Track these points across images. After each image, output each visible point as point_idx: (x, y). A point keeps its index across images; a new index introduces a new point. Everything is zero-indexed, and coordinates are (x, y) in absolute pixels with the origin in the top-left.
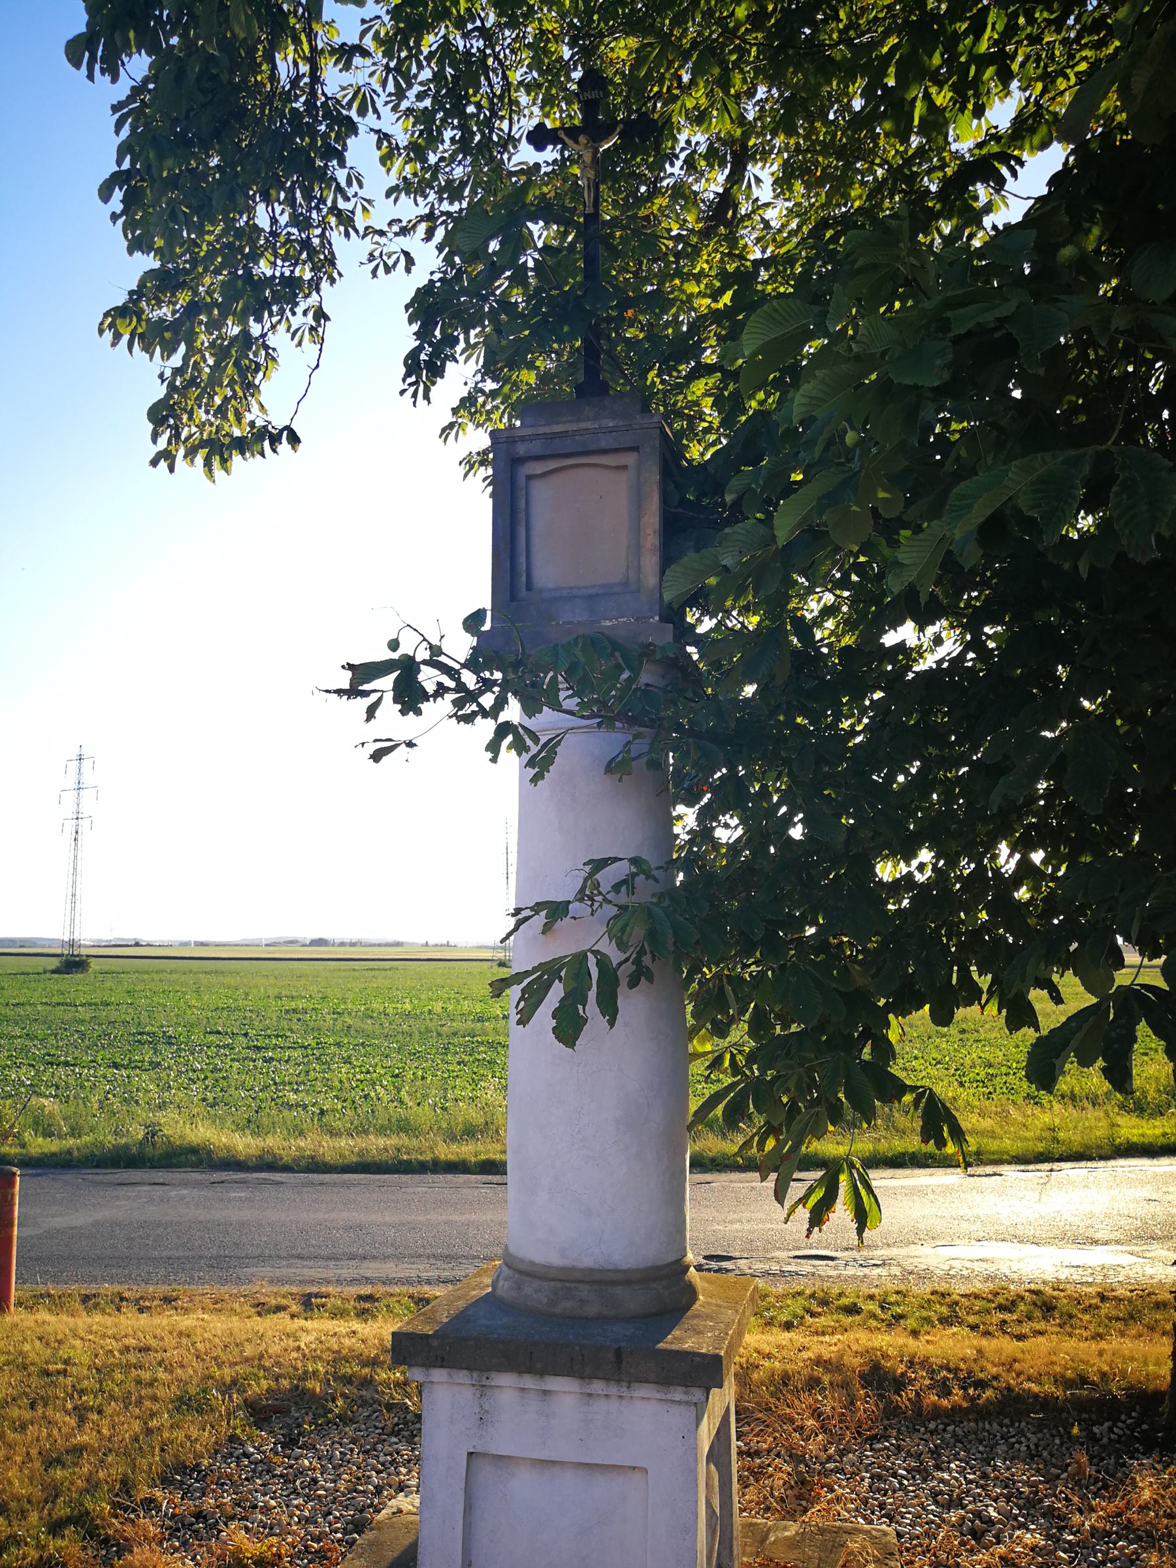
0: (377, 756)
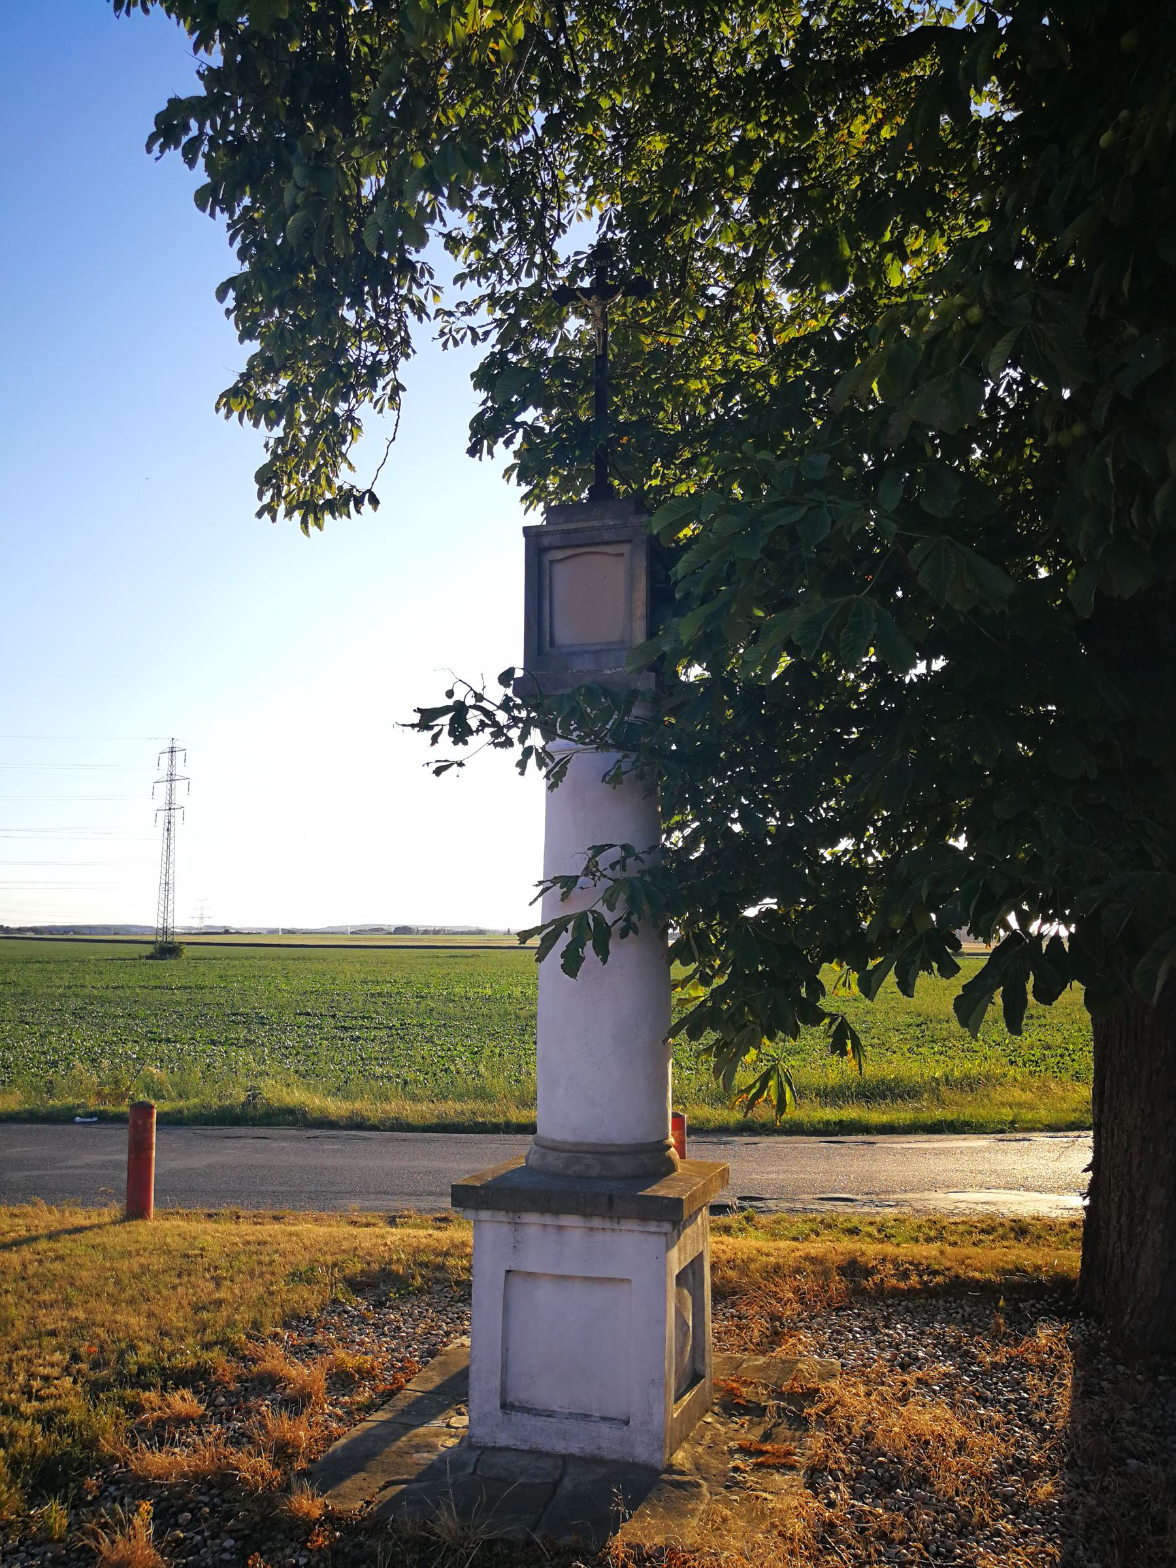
0: (438, 772)
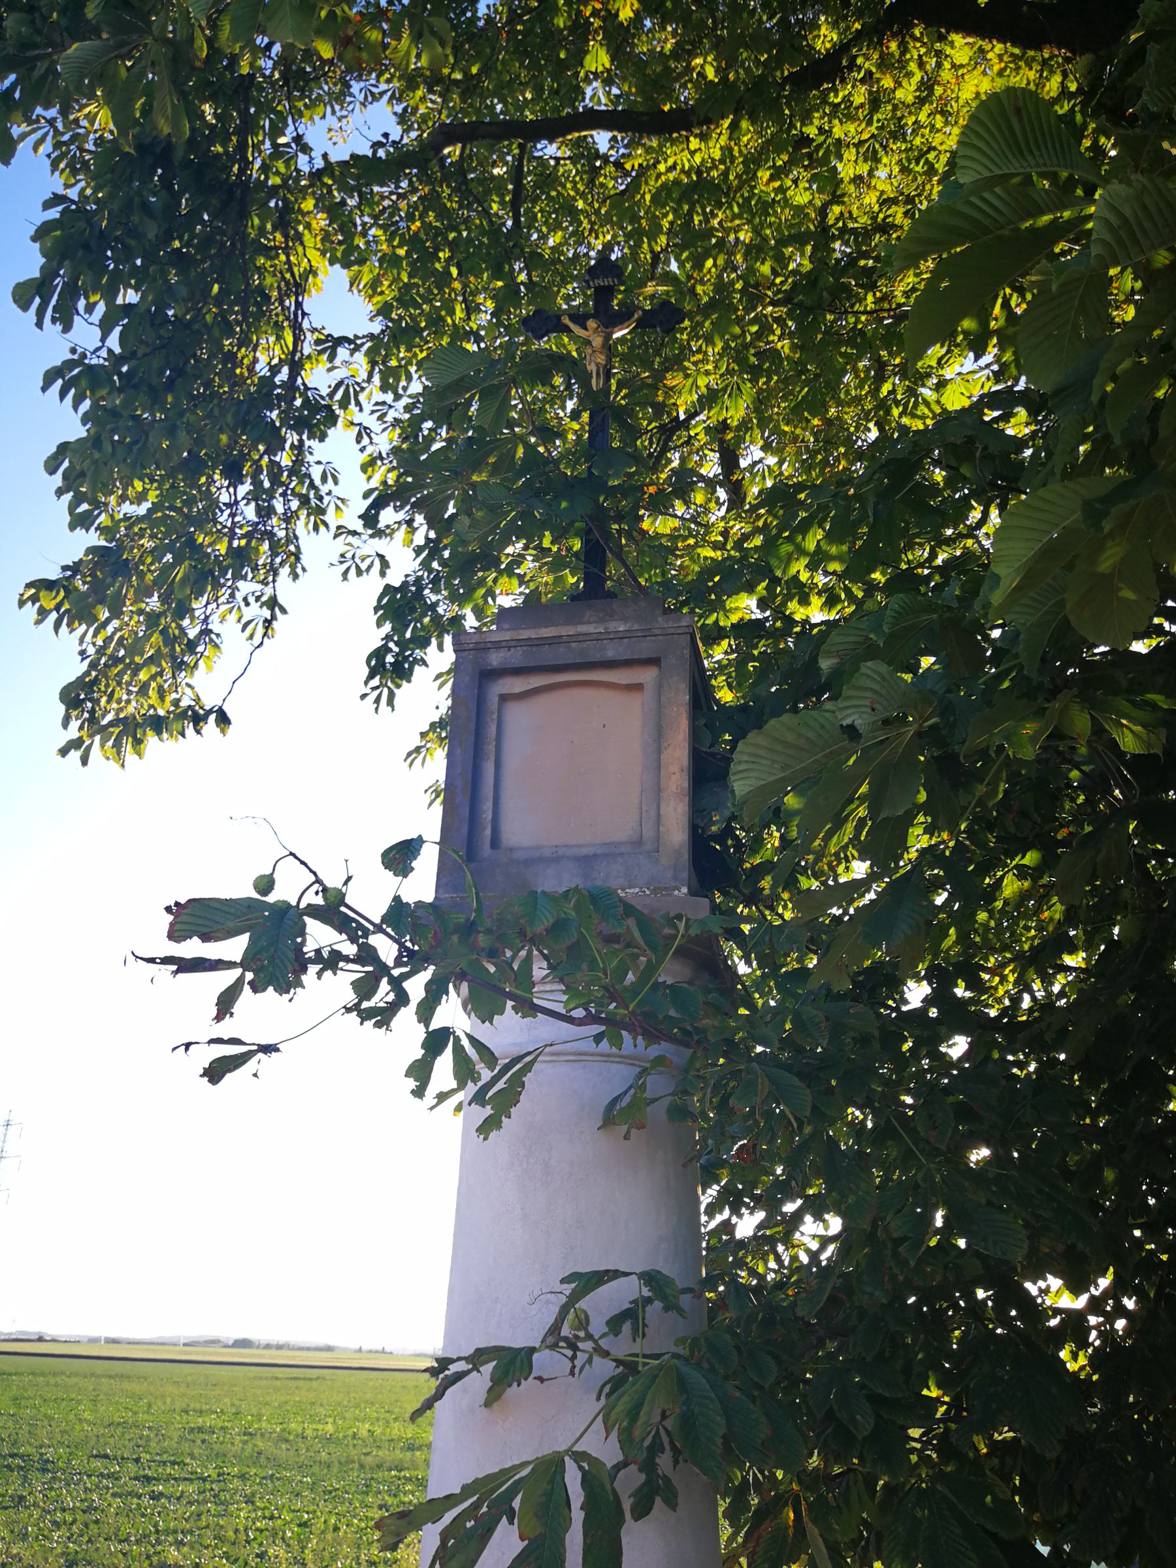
0: (215, 1072)
